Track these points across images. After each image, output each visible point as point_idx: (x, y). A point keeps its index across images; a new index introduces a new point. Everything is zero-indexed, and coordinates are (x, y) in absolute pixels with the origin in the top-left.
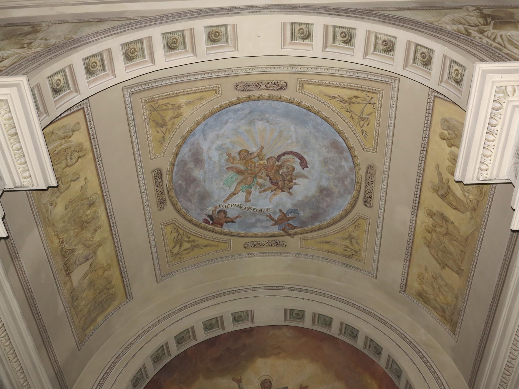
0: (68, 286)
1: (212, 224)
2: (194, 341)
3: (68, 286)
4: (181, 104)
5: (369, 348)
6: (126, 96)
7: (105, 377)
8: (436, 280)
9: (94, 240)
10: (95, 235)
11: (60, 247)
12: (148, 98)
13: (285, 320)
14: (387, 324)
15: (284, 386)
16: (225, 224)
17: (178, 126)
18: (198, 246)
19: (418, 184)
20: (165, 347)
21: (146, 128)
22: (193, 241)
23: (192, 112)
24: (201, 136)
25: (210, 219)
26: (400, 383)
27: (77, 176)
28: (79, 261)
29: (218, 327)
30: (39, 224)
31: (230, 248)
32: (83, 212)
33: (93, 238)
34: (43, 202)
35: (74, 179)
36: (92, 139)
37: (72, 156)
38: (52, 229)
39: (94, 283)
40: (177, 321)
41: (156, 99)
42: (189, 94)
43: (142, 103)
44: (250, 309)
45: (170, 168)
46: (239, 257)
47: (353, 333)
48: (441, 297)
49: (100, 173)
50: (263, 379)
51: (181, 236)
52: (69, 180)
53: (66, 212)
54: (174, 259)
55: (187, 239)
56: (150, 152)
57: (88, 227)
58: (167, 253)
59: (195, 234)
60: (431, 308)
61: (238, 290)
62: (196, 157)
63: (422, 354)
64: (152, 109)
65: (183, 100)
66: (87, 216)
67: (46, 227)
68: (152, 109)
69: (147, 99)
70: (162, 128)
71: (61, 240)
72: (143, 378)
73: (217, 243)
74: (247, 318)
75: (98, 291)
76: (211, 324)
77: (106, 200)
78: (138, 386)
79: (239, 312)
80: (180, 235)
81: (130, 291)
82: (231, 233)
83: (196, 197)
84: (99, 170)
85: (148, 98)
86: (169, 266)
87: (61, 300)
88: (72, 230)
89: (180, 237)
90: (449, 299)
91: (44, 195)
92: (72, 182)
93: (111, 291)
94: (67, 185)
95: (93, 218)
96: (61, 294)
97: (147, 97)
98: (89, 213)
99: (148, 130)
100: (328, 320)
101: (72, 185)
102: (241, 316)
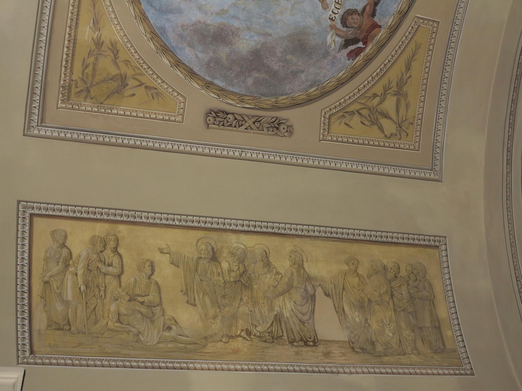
0: (335, 350)
1: (365, 43)
3: (335, 350)
4: (93, 39)
6: (42, 133)
9: (282, 271)
10: (275, 267)
11: (256, 340)
12: (61, 96)
16: (376, 19)
17: (135, 55)
18: (401, 83)
21: (117, 114)
22: (386, 89)
23: (116, 23)
24: (169, 17)
25: (353, 44)
27: (148, 263)
28: (304, 315)
30: (186, 363)
31: (434, 21)
32: (219, 275)
33: (278, 273)
34: (155, 343)
35: (150, 272)
36: (95, 217)
37: (107, 261)
38: (212, 344)
41: (68, 81)
42: (77, 19)
43: (66, 108)
45: (214, 93)
46: (461, 10)
49: (164, 222)
51: (364, 108)
52: (145, 281)
53: (199, 307)
54: (407, 135)
55: (377, 99)
56: (166, 120)
57: (252, 275)
58: (387, 144)
59: (372, 83)
62: (210, 39)
64: (84, 94)
65: (87, 33)
66: (230, 271)
67: (201, 352)
68: (84, 94)
69: (63, 97)
70: (127, 85)
71: (243, 334)
73: (412, 45)
75: (387, 298)
77: (222, 226)
80: (361, 112)
82: (400, 12)
83: (295, 60)
84: (158, 221)
85: (61, 96)
86: (417, 148)
87: (351, 373)
88: (238, 307)
89: (365, 112)
91: (143, 337)
92: (152, 277)
94: (153, 287)
95: (241, 261)
96: (341, 370)
97: (59, 96)
98: (227, 265)
99: (122, 113)
101: (159, 280)
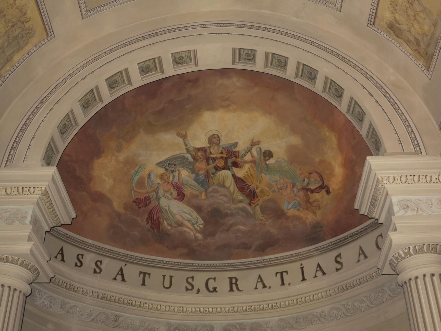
2: (129, 85)
5: (329, 91)
7: (27, 122)
8: (412, 5)
13: (234, 62)
14: (351, 63)
15: (234, 142)
19: (370, 23)
20: (95, 91)
26: (362, 128)
29: (156, 70)
39: (4, 13)
40: (108, 62)
44: (193, 49)
47: (311, 74)
48: (417, 26)
50: (211, 134)
60: (403, 42)
61: (179, 28)
63: (389, 95)
72: (72, 125)
74: (189, 60)
75: (10, 24)
76: (148, 66)
78: (67, 133)
79: (179, 52)
81: (50, 27)
90: (426, 27)
93: (27, 25)
100: (282, 60)
102: (183, 58)
